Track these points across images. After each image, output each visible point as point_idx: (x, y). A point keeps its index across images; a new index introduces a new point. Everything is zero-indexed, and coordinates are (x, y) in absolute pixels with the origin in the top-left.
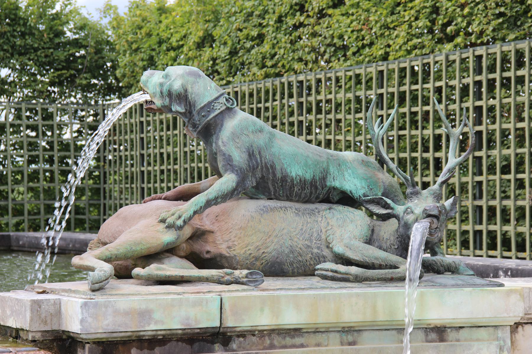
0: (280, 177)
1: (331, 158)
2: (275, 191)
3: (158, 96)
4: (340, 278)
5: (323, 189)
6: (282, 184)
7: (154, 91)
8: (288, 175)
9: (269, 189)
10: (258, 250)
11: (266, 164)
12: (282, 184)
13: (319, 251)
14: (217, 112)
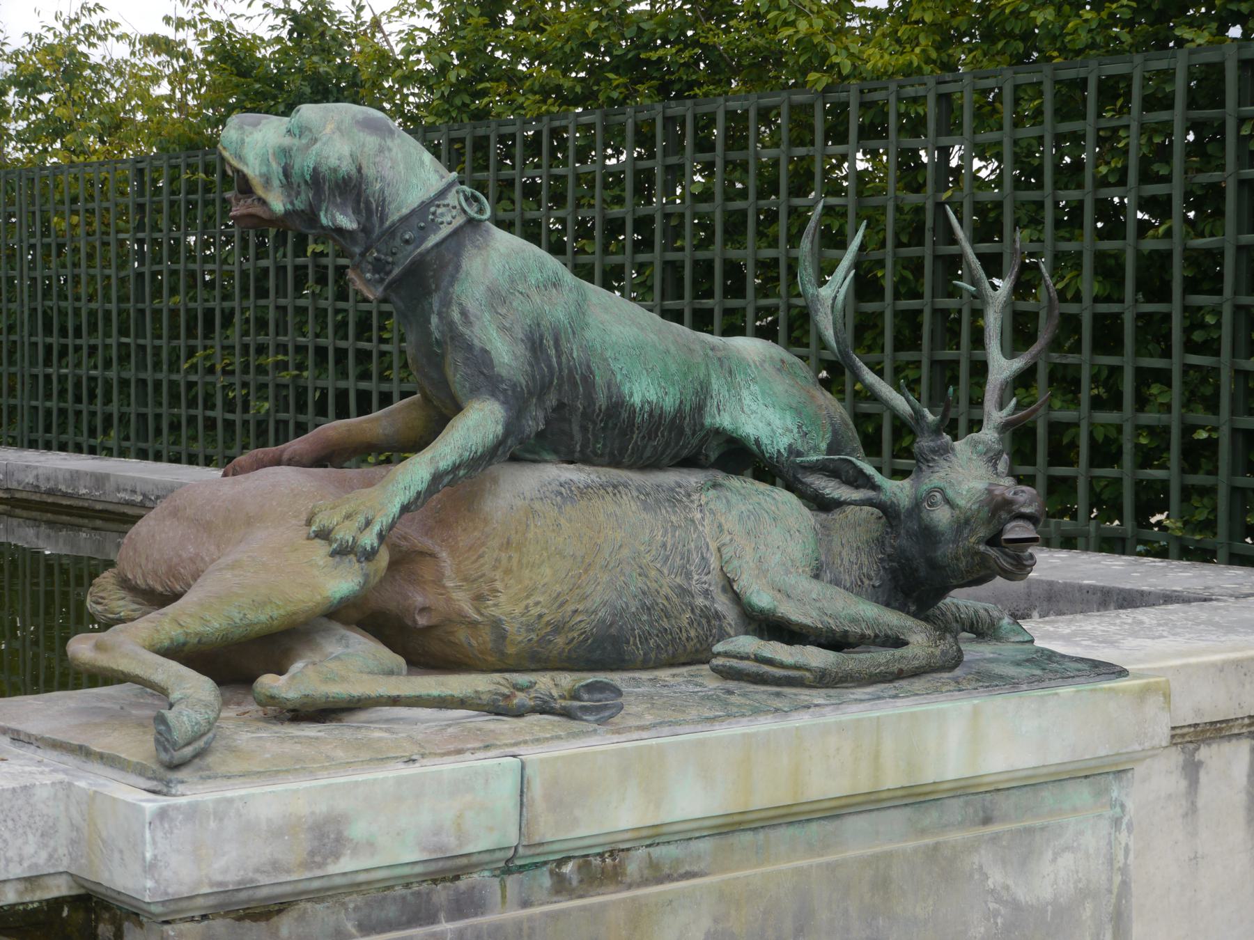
0: (603, 407)
1: (711, 353)
2: (584, 447)
3: (276, 183)
4: (780, 678)
5: (693, 435)
6: (606, 424)
7: (264, 169)
8: (623, 402)
9: (572, 437)
11: (570, 371)
12: (606, 424)
13: (707, 603)
14: (445, 231)
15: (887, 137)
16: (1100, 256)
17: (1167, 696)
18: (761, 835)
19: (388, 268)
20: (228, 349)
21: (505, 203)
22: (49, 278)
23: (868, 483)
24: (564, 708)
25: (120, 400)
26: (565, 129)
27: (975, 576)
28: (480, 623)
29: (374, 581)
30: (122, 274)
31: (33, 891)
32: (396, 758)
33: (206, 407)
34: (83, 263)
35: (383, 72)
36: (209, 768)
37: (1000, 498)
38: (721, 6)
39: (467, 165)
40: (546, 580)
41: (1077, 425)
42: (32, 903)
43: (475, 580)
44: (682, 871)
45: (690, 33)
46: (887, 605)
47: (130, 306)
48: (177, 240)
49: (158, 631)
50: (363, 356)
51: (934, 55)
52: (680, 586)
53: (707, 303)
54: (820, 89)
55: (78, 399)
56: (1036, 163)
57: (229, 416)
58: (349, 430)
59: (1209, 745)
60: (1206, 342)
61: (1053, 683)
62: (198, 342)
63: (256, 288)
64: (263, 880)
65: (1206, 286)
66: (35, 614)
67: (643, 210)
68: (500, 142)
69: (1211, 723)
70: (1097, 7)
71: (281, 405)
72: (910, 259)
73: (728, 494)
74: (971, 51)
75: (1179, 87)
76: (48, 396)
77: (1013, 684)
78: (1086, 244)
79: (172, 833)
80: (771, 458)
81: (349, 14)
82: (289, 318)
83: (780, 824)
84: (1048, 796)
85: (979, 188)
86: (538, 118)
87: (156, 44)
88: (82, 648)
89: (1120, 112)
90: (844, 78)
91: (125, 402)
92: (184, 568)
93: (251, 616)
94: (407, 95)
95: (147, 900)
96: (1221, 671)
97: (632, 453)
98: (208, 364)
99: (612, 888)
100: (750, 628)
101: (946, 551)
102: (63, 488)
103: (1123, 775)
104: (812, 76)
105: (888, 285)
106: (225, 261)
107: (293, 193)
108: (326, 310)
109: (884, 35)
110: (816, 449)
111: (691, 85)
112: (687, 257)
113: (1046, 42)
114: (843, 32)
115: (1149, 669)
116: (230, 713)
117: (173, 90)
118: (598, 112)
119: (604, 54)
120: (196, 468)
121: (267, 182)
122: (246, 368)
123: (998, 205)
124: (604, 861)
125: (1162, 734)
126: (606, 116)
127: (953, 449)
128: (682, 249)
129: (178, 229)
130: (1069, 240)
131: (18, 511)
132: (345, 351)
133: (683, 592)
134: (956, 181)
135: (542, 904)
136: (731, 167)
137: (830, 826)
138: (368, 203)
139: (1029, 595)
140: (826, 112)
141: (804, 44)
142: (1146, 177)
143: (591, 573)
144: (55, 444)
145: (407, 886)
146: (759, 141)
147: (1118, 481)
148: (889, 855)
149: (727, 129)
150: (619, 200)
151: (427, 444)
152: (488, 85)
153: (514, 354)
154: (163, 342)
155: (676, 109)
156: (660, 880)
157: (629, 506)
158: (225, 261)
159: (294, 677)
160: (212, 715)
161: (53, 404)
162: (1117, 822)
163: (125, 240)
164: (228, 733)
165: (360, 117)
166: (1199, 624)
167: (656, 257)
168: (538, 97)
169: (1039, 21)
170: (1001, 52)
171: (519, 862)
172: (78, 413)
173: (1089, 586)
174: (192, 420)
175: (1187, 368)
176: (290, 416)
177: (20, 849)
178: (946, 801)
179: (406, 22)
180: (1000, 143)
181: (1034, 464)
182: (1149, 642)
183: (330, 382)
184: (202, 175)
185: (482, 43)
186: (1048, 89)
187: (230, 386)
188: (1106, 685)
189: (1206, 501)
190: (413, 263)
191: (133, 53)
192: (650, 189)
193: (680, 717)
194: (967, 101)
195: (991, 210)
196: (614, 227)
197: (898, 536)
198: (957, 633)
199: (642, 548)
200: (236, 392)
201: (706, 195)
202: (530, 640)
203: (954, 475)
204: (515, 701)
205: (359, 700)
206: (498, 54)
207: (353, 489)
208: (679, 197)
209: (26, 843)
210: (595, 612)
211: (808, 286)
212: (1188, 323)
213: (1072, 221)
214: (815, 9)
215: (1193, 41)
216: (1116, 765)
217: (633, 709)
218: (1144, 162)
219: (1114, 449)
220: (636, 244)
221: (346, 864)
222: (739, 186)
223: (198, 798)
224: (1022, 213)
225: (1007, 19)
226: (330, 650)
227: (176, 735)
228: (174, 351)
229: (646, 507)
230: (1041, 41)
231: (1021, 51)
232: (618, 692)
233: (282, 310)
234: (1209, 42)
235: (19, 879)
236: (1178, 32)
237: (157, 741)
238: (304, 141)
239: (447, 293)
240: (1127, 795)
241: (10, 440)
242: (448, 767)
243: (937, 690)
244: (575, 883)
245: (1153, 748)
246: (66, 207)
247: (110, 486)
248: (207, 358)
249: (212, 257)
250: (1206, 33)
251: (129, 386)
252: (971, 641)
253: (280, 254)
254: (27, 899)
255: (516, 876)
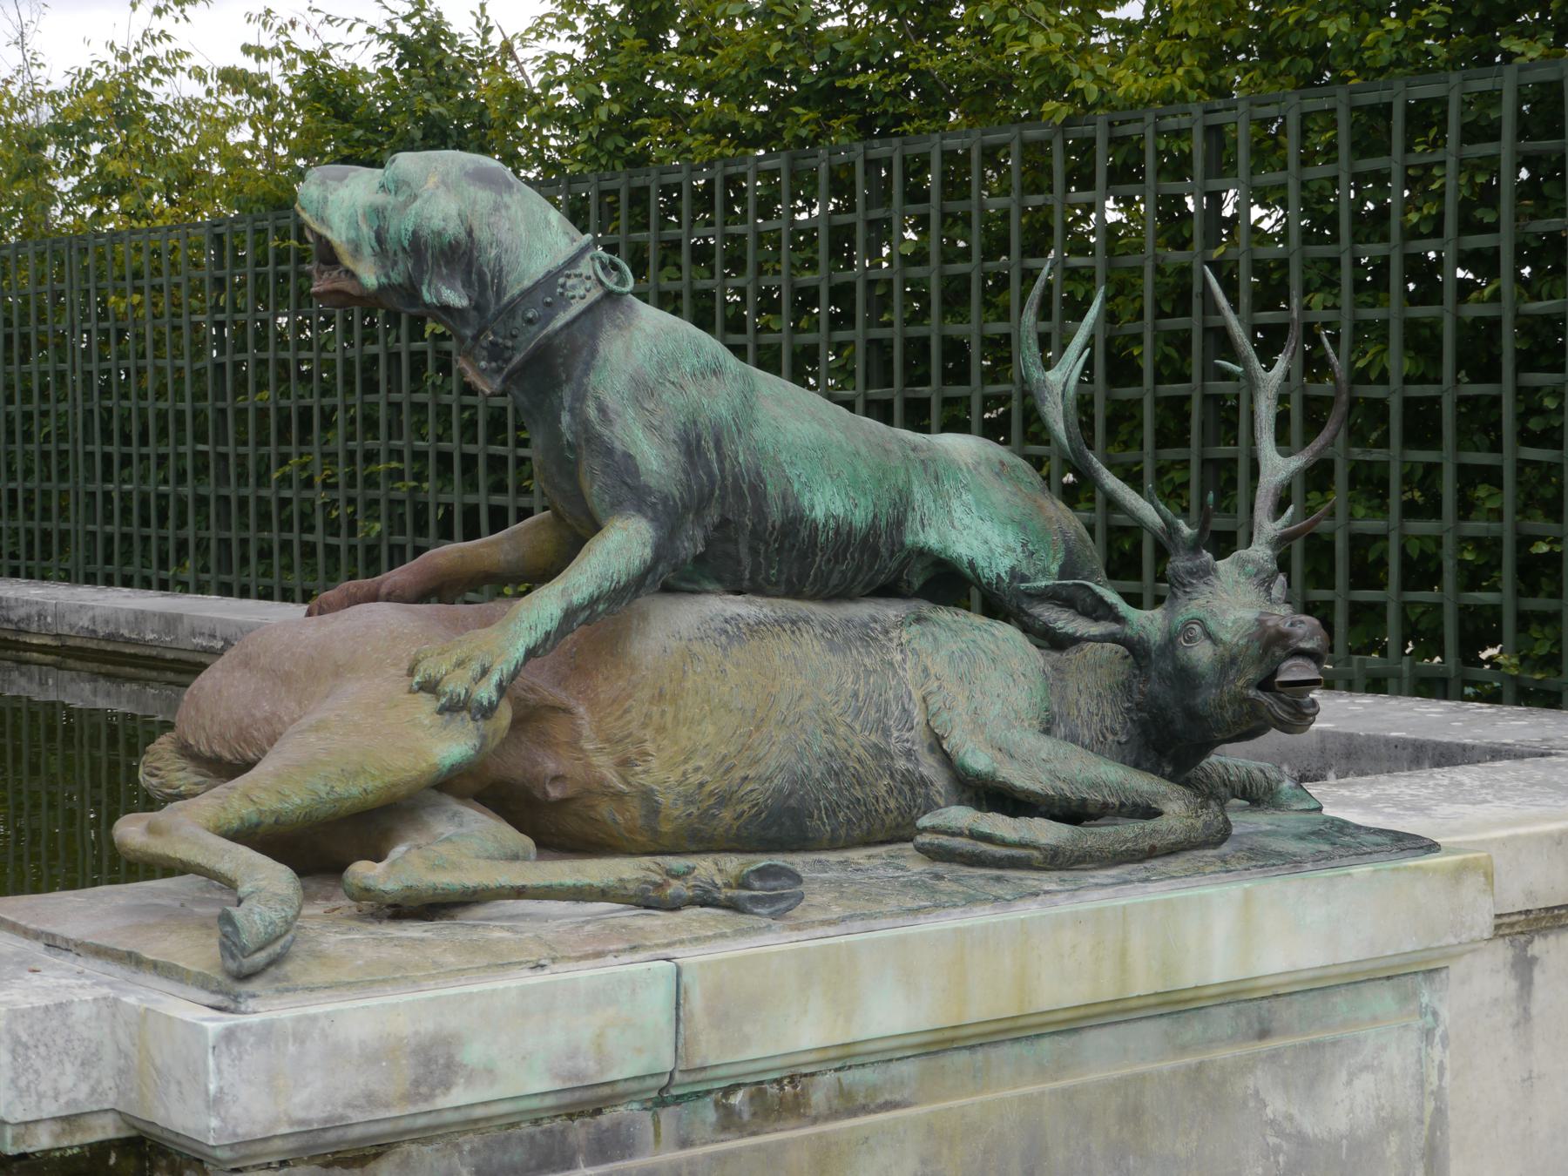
0: (778, 524)
1: (912, 455)
3: (367, 251)
4: (1001, 859)
5: (892, 554)
7: (352, 234)
8: (802, 517)
9: (739, 562)
10: (727, 771)
11: (736, 479)
13: (910, 766)
14: (577, 307)
15: (1143, 182)
16: (1411, 326)
17: (1489, 876)
18: (980, 1055)
19: (507, 354)
20: (330, 457)
21: (670, 270)
22: (108, 372)
23: (1110, 613)
24: (730, 899)
25: (197, 523)
26: (744, 177)
27: (1245, 728)
28: (625, 794)
29: (493, 743)
30: (198, 365)
31: (72, 1133)
32: (520, 963)
33: (303, 530)
34: (149, 353)
35: (516, 109)
36: (286, 978)
37: (1273, 631)
38: (935, 20)
39: (623, 223)
40: (708, 740)
41: (1386, 537)
42: (71, 1148)
43: (620, 741)
44: (881, 1100)
45: (897, 54)
46: (1137, 765)
47: (208, 405)
48: (265, 323)
49: (225, 809)
50: (497, 463)
51: (1201, 77)
52: (875, 745)
53: (922, 391)
54: (1058, 122)
55: (145, 522)
56: (1329, 210)
57: (332, 541)
58: (462, 557)
59: (1545, 936)
60: (1544, 432)
61: (1345, 861)
62: (293, 449)
63: (364, 381)
64: (356, 1116)
65: (1544, 361)
66: (96, 785)
67: (842, 277)
68: (662, 195)
69: (1547, 909)
70: (1404, 14)
71: (397, 525)
72: (1174, 333)
73: (936, 630)
74: (1247, 71)
75: (1506, 113)
76: (108, 519)
77: (1293, 863)
78: (1393, 311)
79: (241, 1059)
80: (989, 584)
81: (474, 37)
82: (405, 417)
83: (1003, 1041)
84: (1341, 1002)
85: (1259, 243)
86: (710, 164)
87: (233, 79)
88: (131, 831)
89: (1434, 145)
90: (1088, 108)
91: (203, 525)
92: (258, 730)
93: (340, 789)
94: (547, 137)
95: (212, 1142)
96: (1559, 843)
97: (815, 580)
98: (305, 475)
99: (793, 1122)
100: (965, 796)
101: (1207, 698)
102: (126, 632)
103: (1436, 975)
104: (1049, 106)
105: (1147, 365)
106: (323, 348)
107: (389, 264)
108: (449, 407)
109: (1138, 54)
110: (1045, 572)
111: (899, 119)
112: (896, 334)
113: (1340, 59)
114: (1086, 49)
115: (1467, 842)
116: (316, 909)
117: (256, 136)
118: (783, 154)
119: (790, 82)
120: (291, 606)
121: (356, 249)
122: (351, 481)
123: (1283, 264)
124: (782, 1089)
125: (1484, 923)
126: (793, 159)
127: (1215, 570)
128: (890, 324)
129: (266, 308)
130: (1373, 306)
131: (71, 663)
132: (474, 457)
133: (880, 752)
134: (1230, 235)
135: (705, 1144)
136: (950, 220)
137: (1065, 1043)
138: (481, 275)
139: (1323, 751)
140: (1068, 151)
141: (1041, 64)
142: (1468, 225)
143: (764, 730)
144: (117, 578)
145: (536, 1122)
146: (985, 188)
147: (1439, 606)
148: (1141, 1078)
149: (944, 173)
150: (813, 265)
151: (559, 572)
152: (648, 121)
153: (665, 459)
154: (249, 450)
155: (879, 150)
156: (853, 1112)
157: (811, 647)
158: (323, 348)
159: (393, 864)
160: (291, 913)
161: (115, 528)
162: (1428, 1034)
163: (199, 323)
164: (312, 934)
165: (470, 167)
166: (1532, 785)
167: (858, 334)
168: (708, 137)
169: (1331, 32)
170: (1284, 73)
171: (675, 1092)
172: (146, 539)
173: (1398, 739)
174: (286, 546)
175: (1522, 465)
176: (407, 539)
177: (55, 1081)
178: (1213, 1010)
179: (546, 46)
180: (1284, 186)
181: (1332, 587)
182: (1469, 809)
183: (457, 496)
184: (293, 242)
185: (639, 71)
186: (1343, 117)
187: (333, 503)
188: (1412, 863)
189: (1548, 630)
190: (538, 347)
191: (209, 93)
192: (851, 250)
193: (876, 908)
194: (1242, 135)
195: (1273, 270)
196: (808, 297)
197: (1148, 680)
198: (1226, 800)
199: (828, 699)
200: (341, 511)
201: (919, 256)
202: (689, 815)
203: (1216, 603)
204: (670, 891)
205: (475, 891)
206: (660, 84)
207: (467, 629)
208: (885, 259)
209: (62, 1073)
210: (770, 779)
211: (1033, 369)
212: (1522, 408)
213: (1374, 284)
214: (1052, 20)
215: (1523, 54)
216: (1427, 962)
217: (817, 900)
218: (1465, 206)
219: (1432, 566)
220: (833, 318)
221: (459, 1096)
222: (961, 244)
223: (274, 1015)
224: (1313, 273)
225: (1292, 30)
226: (440, 830)
227: (245, 938)
228: (263, 461)
229: (832, 647)
230: (1335, 58)
231: (1310, 70)
232: (797, 879)
233: (395, 407)
234: (1544, 56)
235: (54, 1119)
236: (1504, 44)
237: (223, 945)
238: (401, 198)
239: (581, 384)
240: (1440, 1000)
241: (62, 574)
242: (586, 973)
243: (1199, 872)
244: (746, 1117)
245: (1473, 941)
246: (128, 284)
247: (184, 629)
248: (304, 467)
249: (310, 341)
250: (1540, 45)
251: (207, 504)
252: (1243, 809)
253: (391, 339)
254: (65, 1143)
255: (671, 1109)
